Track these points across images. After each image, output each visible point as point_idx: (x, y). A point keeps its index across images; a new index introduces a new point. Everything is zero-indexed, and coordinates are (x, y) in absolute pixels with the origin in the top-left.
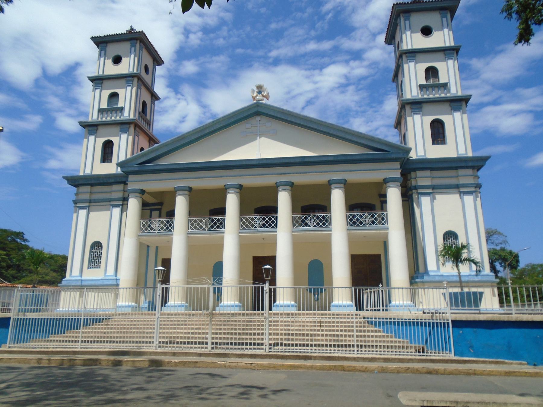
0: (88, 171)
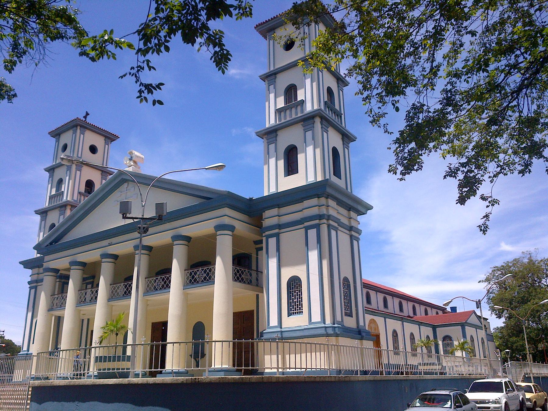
0: (273, 190)
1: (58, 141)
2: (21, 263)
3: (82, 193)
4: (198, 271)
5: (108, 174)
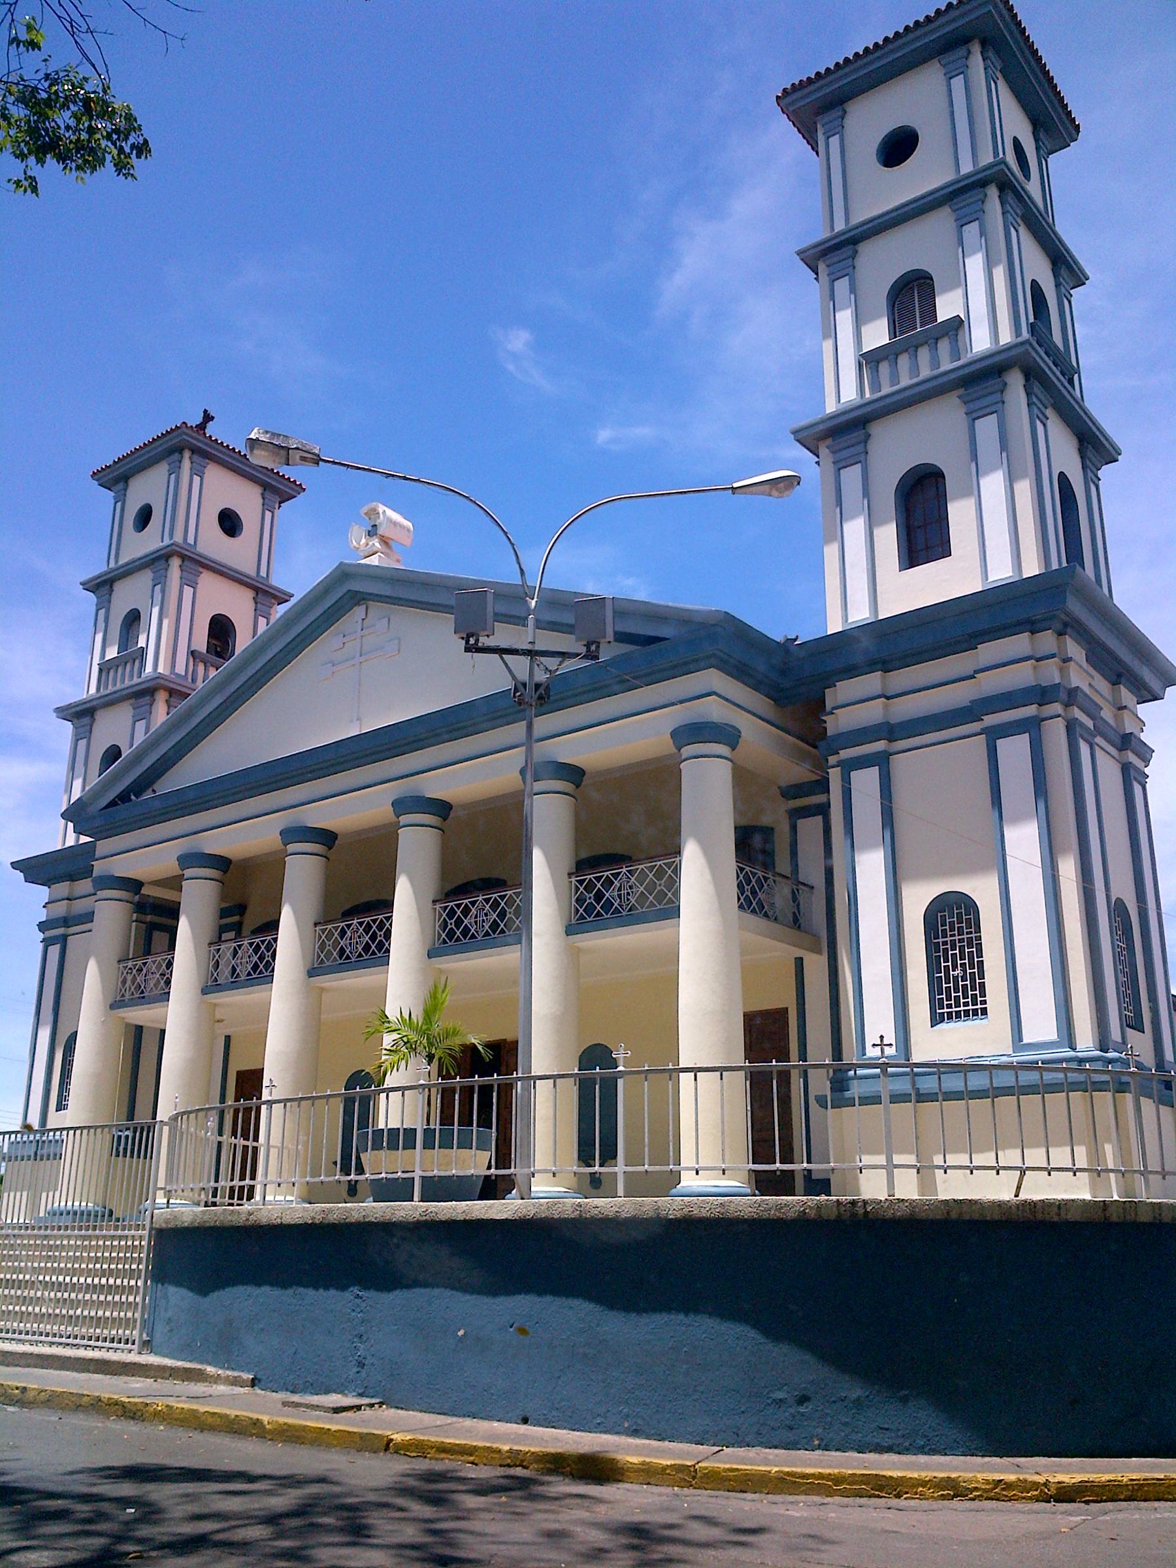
0: (860, 614)
1: (121, 498)
2: (15, 865)
3: (200, 653)
4: (616, 875)
5: (273, 601)
